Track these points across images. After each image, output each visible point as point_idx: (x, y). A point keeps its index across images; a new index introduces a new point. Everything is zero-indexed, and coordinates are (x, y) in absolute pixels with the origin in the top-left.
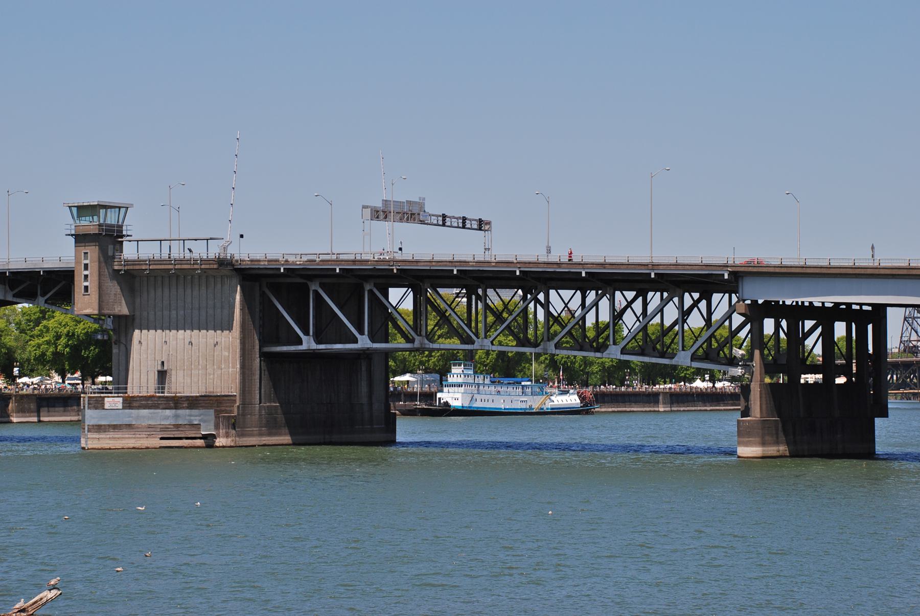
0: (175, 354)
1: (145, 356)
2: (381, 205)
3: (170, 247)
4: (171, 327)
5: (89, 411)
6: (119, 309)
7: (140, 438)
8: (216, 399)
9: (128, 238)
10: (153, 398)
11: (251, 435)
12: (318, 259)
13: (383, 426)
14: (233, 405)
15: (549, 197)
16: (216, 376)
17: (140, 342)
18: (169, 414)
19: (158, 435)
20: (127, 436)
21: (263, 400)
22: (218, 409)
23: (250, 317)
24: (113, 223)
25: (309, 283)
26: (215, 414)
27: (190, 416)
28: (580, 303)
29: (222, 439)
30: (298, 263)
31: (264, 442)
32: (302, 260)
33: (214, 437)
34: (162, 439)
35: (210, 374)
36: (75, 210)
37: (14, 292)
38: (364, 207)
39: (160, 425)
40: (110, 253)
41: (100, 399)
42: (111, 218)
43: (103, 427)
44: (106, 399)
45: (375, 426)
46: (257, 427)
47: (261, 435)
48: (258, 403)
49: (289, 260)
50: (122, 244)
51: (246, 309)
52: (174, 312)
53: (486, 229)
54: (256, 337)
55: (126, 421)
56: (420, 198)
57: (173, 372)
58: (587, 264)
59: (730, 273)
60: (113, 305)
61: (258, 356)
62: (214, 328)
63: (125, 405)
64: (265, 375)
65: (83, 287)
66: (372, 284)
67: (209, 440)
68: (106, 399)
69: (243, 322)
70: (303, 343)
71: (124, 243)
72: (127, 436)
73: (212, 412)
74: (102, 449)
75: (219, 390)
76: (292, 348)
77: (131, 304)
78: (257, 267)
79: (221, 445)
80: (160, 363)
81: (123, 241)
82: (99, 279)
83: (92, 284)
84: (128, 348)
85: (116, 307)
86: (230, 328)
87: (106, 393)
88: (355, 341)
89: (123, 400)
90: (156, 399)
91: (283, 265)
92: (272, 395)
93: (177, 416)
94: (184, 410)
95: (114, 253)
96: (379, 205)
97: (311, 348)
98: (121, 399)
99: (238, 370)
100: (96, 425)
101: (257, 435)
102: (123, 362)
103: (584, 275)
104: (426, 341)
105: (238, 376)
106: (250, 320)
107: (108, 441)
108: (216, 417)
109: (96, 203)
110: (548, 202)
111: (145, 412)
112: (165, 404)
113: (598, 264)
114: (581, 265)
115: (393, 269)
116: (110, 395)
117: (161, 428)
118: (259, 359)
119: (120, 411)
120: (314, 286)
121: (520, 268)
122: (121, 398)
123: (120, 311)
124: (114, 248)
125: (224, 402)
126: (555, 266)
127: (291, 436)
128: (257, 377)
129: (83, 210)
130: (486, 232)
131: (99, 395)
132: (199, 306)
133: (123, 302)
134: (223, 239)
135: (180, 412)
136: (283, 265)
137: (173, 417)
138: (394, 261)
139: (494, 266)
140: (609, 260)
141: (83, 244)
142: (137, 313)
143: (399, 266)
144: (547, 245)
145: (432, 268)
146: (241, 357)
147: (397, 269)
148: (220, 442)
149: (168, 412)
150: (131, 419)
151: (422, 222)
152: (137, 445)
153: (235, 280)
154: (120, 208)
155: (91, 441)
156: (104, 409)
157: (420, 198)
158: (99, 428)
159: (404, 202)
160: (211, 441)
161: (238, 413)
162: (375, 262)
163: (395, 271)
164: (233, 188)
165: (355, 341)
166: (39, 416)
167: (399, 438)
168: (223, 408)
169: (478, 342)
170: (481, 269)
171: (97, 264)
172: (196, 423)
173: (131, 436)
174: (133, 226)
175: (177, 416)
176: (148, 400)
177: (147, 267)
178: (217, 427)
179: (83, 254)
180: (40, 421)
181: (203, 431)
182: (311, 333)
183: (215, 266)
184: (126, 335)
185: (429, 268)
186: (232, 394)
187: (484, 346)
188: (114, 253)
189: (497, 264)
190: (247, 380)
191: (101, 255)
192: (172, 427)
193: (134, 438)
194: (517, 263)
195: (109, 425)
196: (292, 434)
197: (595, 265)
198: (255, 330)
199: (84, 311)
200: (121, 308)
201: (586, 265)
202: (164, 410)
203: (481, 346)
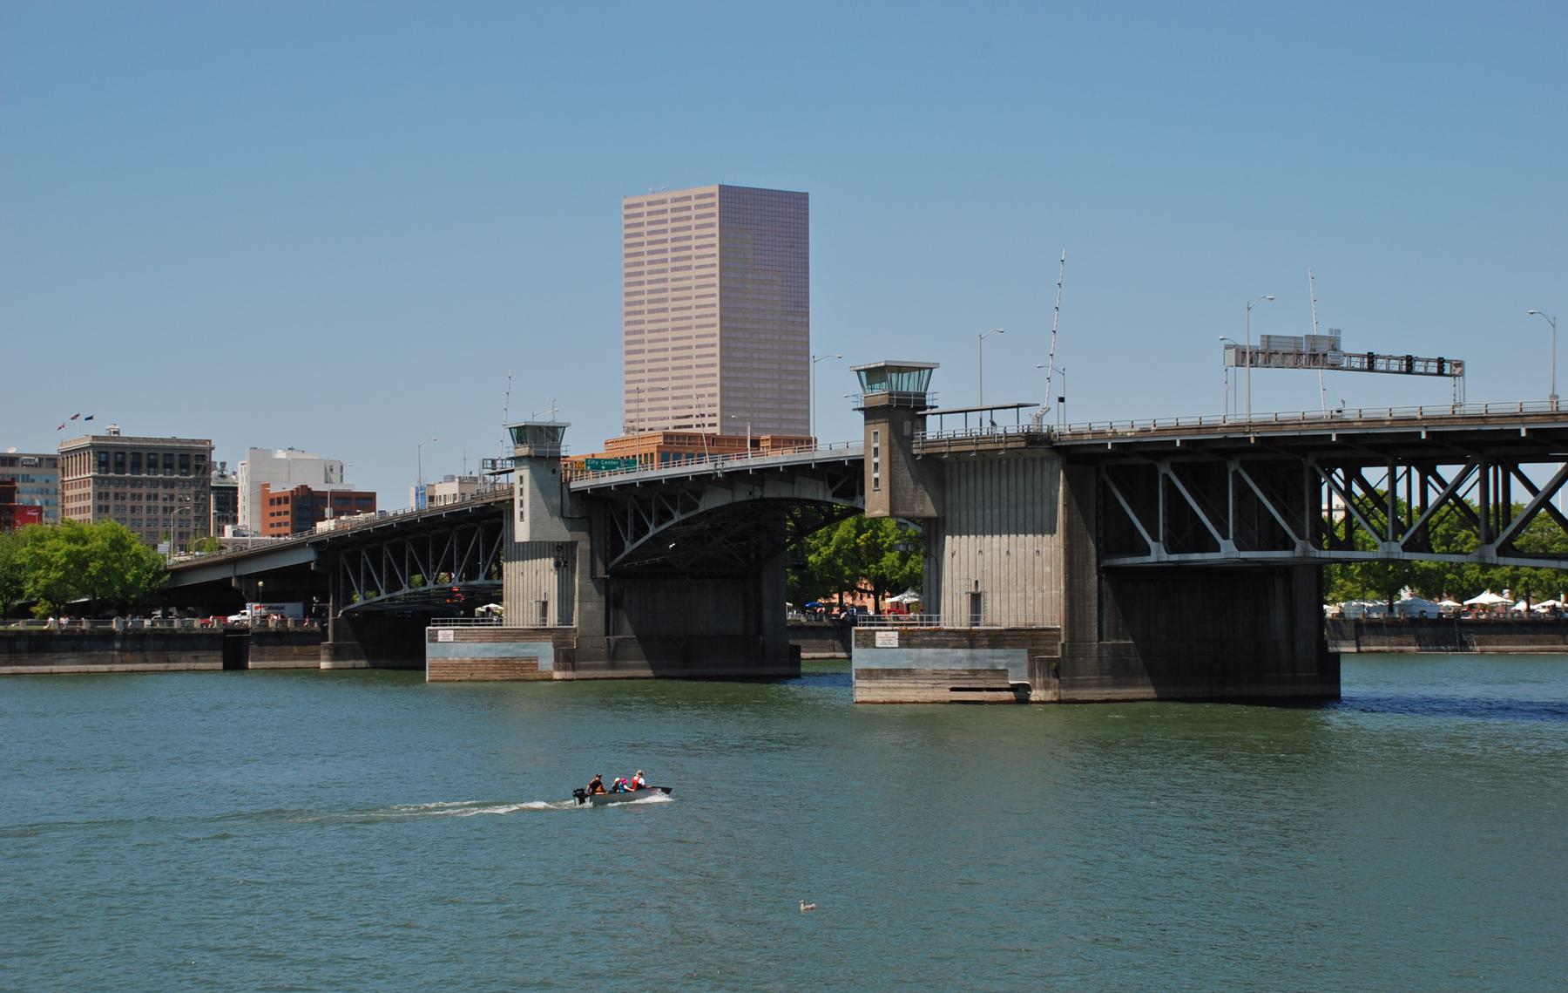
0: (990, 570)
1: (957, 574)
2: (1259, 344)
3: (981, 420)
4: (1002, 531)
5: (857, 649)
6: (921, 509)
7: (923, 688)
8: (1029, 633)
9: (934, 411)
10: (939, 633)
11: (1086, 686)
12: (1153, 428)
13: (1315, 674)
14: (1055, 642)
15: (1554, 318)
16: (1036, 601)
17: (1008, 552)
18: (962, 655)
19: (948, 684)
20: (905, 685)
21: (1105, 636)
22: (1034, 648)
23: (1080, 516)
24: (911, 390)
25: (1157, 464)
26: (1029, 656)
27: (993, 658)
28: (1398, 484)
29: (1038, 692)
30: (1129, 434)
31: (1108, 696)
32: (1133, 430)
33: (1027, 688)
34: (953, 689)
35: (1030, 598)
36: (863, 374)
37: (834, 489)
38: (1227, 347)
39: (950, 670)
40: (907, 432)
41: (870, 634)
42: (909, 384)
43: (875, 673)
44: (877, 633)
45: (1300, 674)
46: (1095, 675)
47: (1102, 685)
48: (1097, 639)
49: (1118, 431)
50: (925, 419)
51: (1074, 504)
52: (988, 511)
53: (1457, 373)
54: (1092, 545)
55: (904, 664)
56: (1331, 331)
57: (988, 596)
58: (1528, 416)
59: (40, 459)
60: (912, 504)
61: (1095, 572)
62: (1042, 529)
63: (902, 642)
64: (1107, 599)
65: (873, 480)
66: (1238, 463)
67: (1021, 692)
68: (877, 633)
69: (1068, 523)
70: (1152, 554)
71: (928, 417)
72: (905, 685)
73: (1024, 652)
74: (873, 703)
75: (1040, 621)
76: (1138, 560)
77: (940, 503)
78: (1080, 443)
79: (1038, 699)
80: (973, 582)
81: (926, 415)
82: (890, 468)
83: (882, 475)
84: (939, 563)
85: (916, 505)
86: (1052, 531)
87: (878, 625)
88: (1217, 548)
89: (899, 636)
90: (943, 634)
91: (1110, 438)
92: (1120, 629)
93: (973, 659)
94: (983, 650)
95: (912, 431)
96: (1256, 342)
97: (1161, 560)
98: (896, 634)
99: (1062, 592)
100: (866, 670)
101: (1095, 686)
102: (933, 582)
103: (1523, 434)
104: (1311, 548)
105: (1062, 601)
106: (1082, 520)
107: (880, 692)
108: (1030, 660)
109: (883, 364)
110: (1554, 326)
111: (928, 652)
112: (956, 641)
113: (1547, 415)
114: (1518, 418)
115: (1249, 438)
116: (882, 628)
117: (951, 675)
118: (1096, 576)
119: (897, 650)
120: (1164, 469)
121: (1426, 427)
122: (897, 633)
123: (922, 511)
124: (913, 425)
125: (1041, 638)
126: (1479, 422)
127: (1155, 688)
128: (1094, 602)
129: (874, 374)
130: (1457, 378)
131: (868, 628)
132: (1016, 501)
133: (928, 498)
134: (1038, 405)
135: (978, 652)
136: (1110, 438)
137: (968, 659)
138: (1251, 426)
139: (1388, 427)
140: (1493, 410)
141: (873, 421)
142: (948, 515)
143: (1258, 433)
144: (1551, 393)
145: (1302, 434)
146: (1065, 574)
147: (1255, 438)
148: (1036, 695)
149: (960, 652)
150: (910, 661)
151: (1334, 367)
152: (920, 697)
153: (1057, 464)
154: (920, 369)
155: (865, 691)
156: (875, 647)
157: (1331, 331)
158: (870, 674)
159: (1302, 338)
160: (1023, 694)
161: (1063, 654)
162: (1226, 429)
163: (1252, 441)
164: (1054, 332)
165: (1217, 548)
166: (1358, 645)
167: (1345, 691)
168: (1041, 648)
169: (1384, 548)
170: (1371, 432)
171: (887, 447)
172: (1001, 668)
173: (911, 685)
174: (939, 393)
175: (973, 659)
176: (932, 636)
177: (973, 447)
178: (1032, 674)
179: (872, 434)
180: (1359, 651)
181: (1012, 679)
182: (1161, 539)
183: (1023, 444)
184: (937, 544)
185: (1297, 434)
186: (1054, 627)
187: (1392, 553)
188: (912, 431)
189: (1394, 422)
190: (1076, 608)
191: (892, 435)
192: (966, 673)
193: (916, 688)
194: (1423, 419)
195: (882, 670)
196: (1155, 685)
197: (1540, 417)
198: (1091, 534)
199: (875, 513)
200: (924, 507)
201: (1527, 418)
202: (955, 650)
203: (1388, 552)
